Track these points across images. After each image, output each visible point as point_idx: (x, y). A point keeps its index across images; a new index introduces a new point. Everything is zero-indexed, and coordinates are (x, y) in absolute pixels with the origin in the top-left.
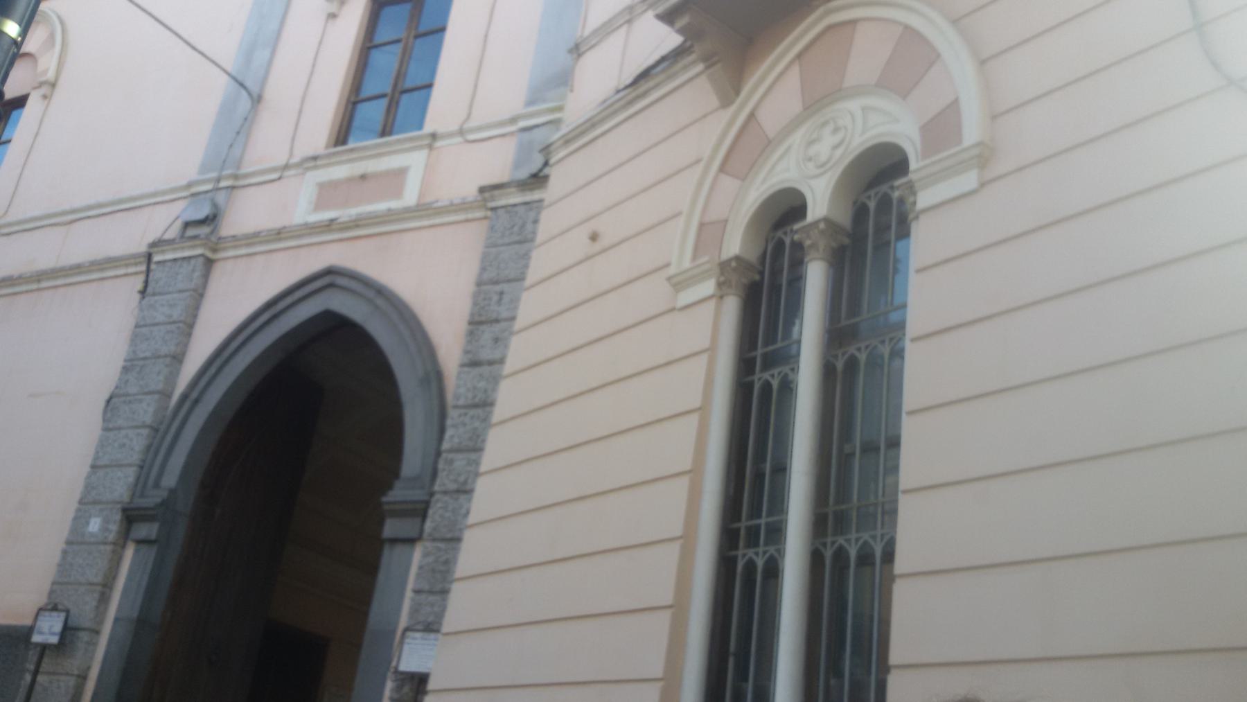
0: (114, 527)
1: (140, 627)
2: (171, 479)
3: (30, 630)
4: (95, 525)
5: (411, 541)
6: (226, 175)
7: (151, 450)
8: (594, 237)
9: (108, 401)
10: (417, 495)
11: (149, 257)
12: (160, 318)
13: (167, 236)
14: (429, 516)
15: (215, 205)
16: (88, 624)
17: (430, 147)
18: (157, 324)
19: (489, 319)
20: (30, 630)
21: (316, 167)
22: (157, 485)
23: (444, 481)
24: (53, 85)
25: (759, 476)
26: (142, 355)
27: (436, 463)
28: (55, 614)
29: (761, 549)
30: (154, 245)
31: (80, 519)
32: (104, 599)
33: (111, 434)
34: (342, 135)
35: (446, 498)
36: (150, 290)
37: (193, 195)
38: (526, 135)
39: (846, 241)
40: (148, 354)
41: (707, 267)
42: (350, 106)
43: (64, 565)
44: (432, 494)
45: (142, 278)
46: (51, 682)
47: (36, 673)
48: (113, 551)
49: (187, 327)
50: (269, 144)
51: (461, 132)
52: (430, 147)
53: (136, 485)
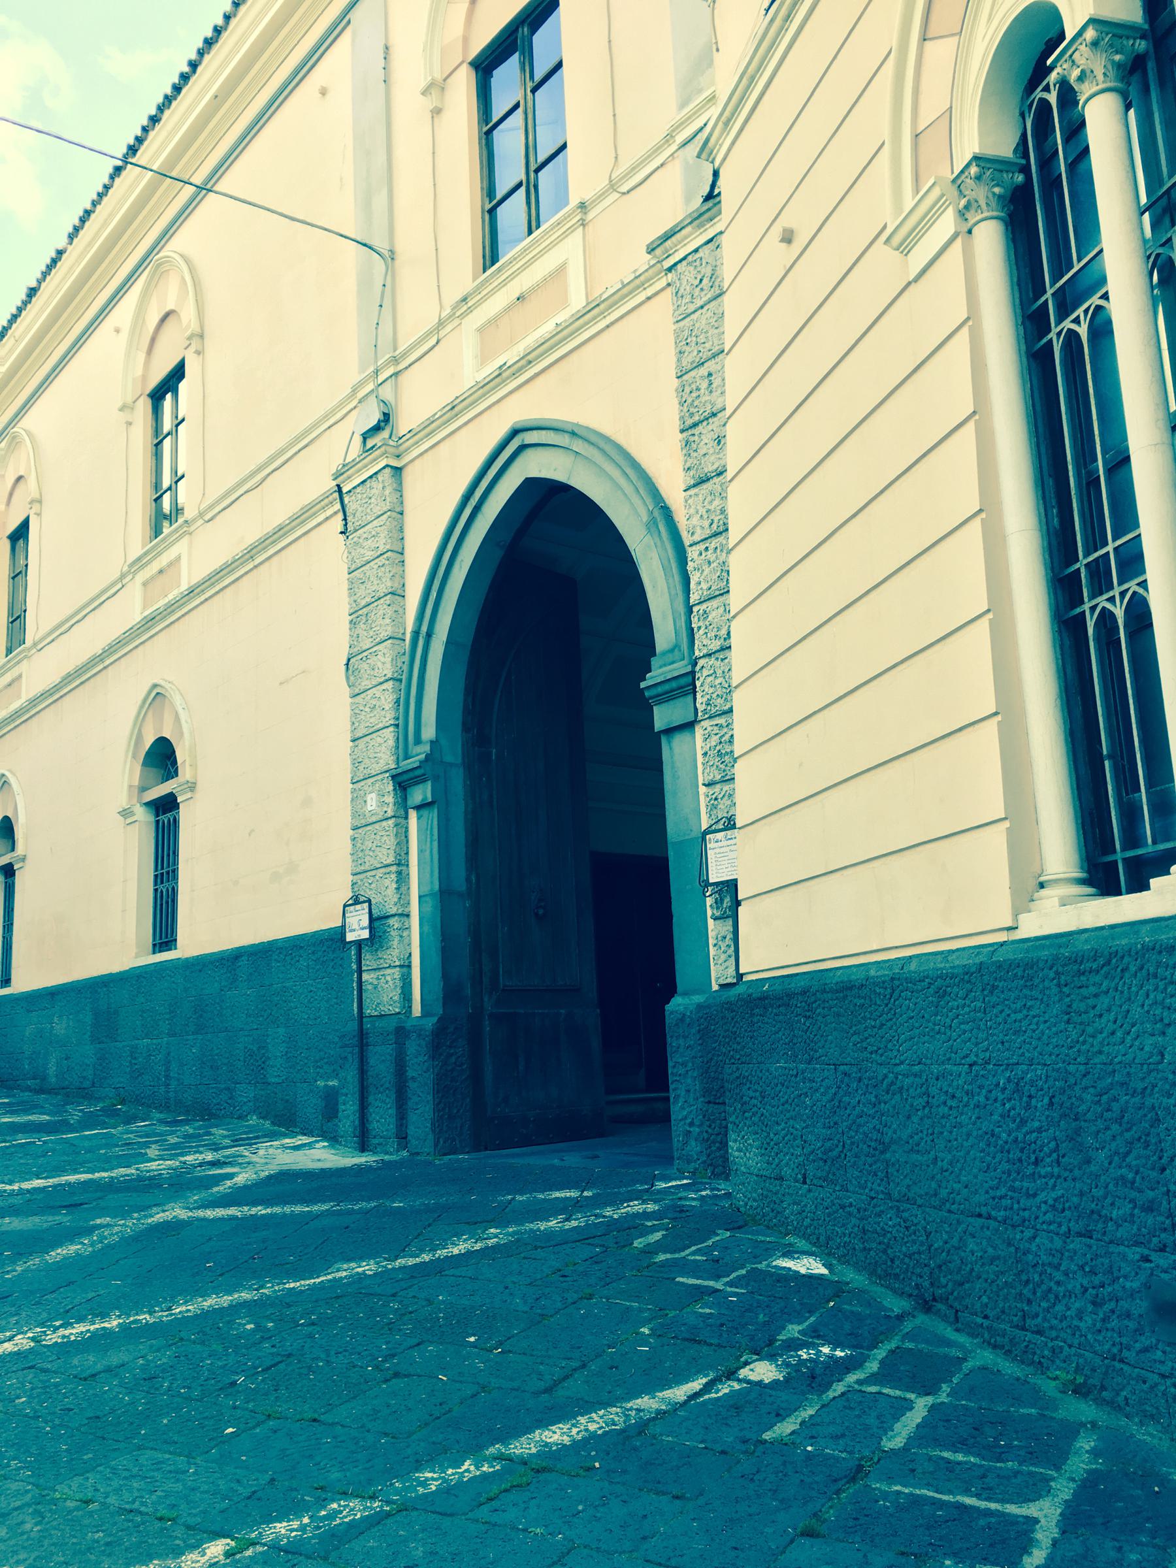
0: (390, 799)
1: (444, 896)
2: (429, 732)
5: (690, 726)
8: (788, 238)
9: (347, 664)
10: (680, 667)
12: (369, 555)
16: (394, 911)
17: (583, 224)
19: (699, 421)
21: (470, 310)
22: (418, 741)
23: (704, 642)
24: (201, 336)
25: (1092, 483)
26: (363, 603)
27: (689, 622)
28: (358, 907)
29: (1116, 592)
31: (357, 798)
32: (402, 879)
33: (359, 699)
34: (491, 255)
35: (712, 661)
36: (350, 527)
39: (1141, 46)
40: (368, 600)
41: (937, 192)
42: (487, 216)
45: (340, 516)
46: (378, 979)
47: (360, 971)
50: (417, 310)
51: (612, 186)
52: (583, 224)
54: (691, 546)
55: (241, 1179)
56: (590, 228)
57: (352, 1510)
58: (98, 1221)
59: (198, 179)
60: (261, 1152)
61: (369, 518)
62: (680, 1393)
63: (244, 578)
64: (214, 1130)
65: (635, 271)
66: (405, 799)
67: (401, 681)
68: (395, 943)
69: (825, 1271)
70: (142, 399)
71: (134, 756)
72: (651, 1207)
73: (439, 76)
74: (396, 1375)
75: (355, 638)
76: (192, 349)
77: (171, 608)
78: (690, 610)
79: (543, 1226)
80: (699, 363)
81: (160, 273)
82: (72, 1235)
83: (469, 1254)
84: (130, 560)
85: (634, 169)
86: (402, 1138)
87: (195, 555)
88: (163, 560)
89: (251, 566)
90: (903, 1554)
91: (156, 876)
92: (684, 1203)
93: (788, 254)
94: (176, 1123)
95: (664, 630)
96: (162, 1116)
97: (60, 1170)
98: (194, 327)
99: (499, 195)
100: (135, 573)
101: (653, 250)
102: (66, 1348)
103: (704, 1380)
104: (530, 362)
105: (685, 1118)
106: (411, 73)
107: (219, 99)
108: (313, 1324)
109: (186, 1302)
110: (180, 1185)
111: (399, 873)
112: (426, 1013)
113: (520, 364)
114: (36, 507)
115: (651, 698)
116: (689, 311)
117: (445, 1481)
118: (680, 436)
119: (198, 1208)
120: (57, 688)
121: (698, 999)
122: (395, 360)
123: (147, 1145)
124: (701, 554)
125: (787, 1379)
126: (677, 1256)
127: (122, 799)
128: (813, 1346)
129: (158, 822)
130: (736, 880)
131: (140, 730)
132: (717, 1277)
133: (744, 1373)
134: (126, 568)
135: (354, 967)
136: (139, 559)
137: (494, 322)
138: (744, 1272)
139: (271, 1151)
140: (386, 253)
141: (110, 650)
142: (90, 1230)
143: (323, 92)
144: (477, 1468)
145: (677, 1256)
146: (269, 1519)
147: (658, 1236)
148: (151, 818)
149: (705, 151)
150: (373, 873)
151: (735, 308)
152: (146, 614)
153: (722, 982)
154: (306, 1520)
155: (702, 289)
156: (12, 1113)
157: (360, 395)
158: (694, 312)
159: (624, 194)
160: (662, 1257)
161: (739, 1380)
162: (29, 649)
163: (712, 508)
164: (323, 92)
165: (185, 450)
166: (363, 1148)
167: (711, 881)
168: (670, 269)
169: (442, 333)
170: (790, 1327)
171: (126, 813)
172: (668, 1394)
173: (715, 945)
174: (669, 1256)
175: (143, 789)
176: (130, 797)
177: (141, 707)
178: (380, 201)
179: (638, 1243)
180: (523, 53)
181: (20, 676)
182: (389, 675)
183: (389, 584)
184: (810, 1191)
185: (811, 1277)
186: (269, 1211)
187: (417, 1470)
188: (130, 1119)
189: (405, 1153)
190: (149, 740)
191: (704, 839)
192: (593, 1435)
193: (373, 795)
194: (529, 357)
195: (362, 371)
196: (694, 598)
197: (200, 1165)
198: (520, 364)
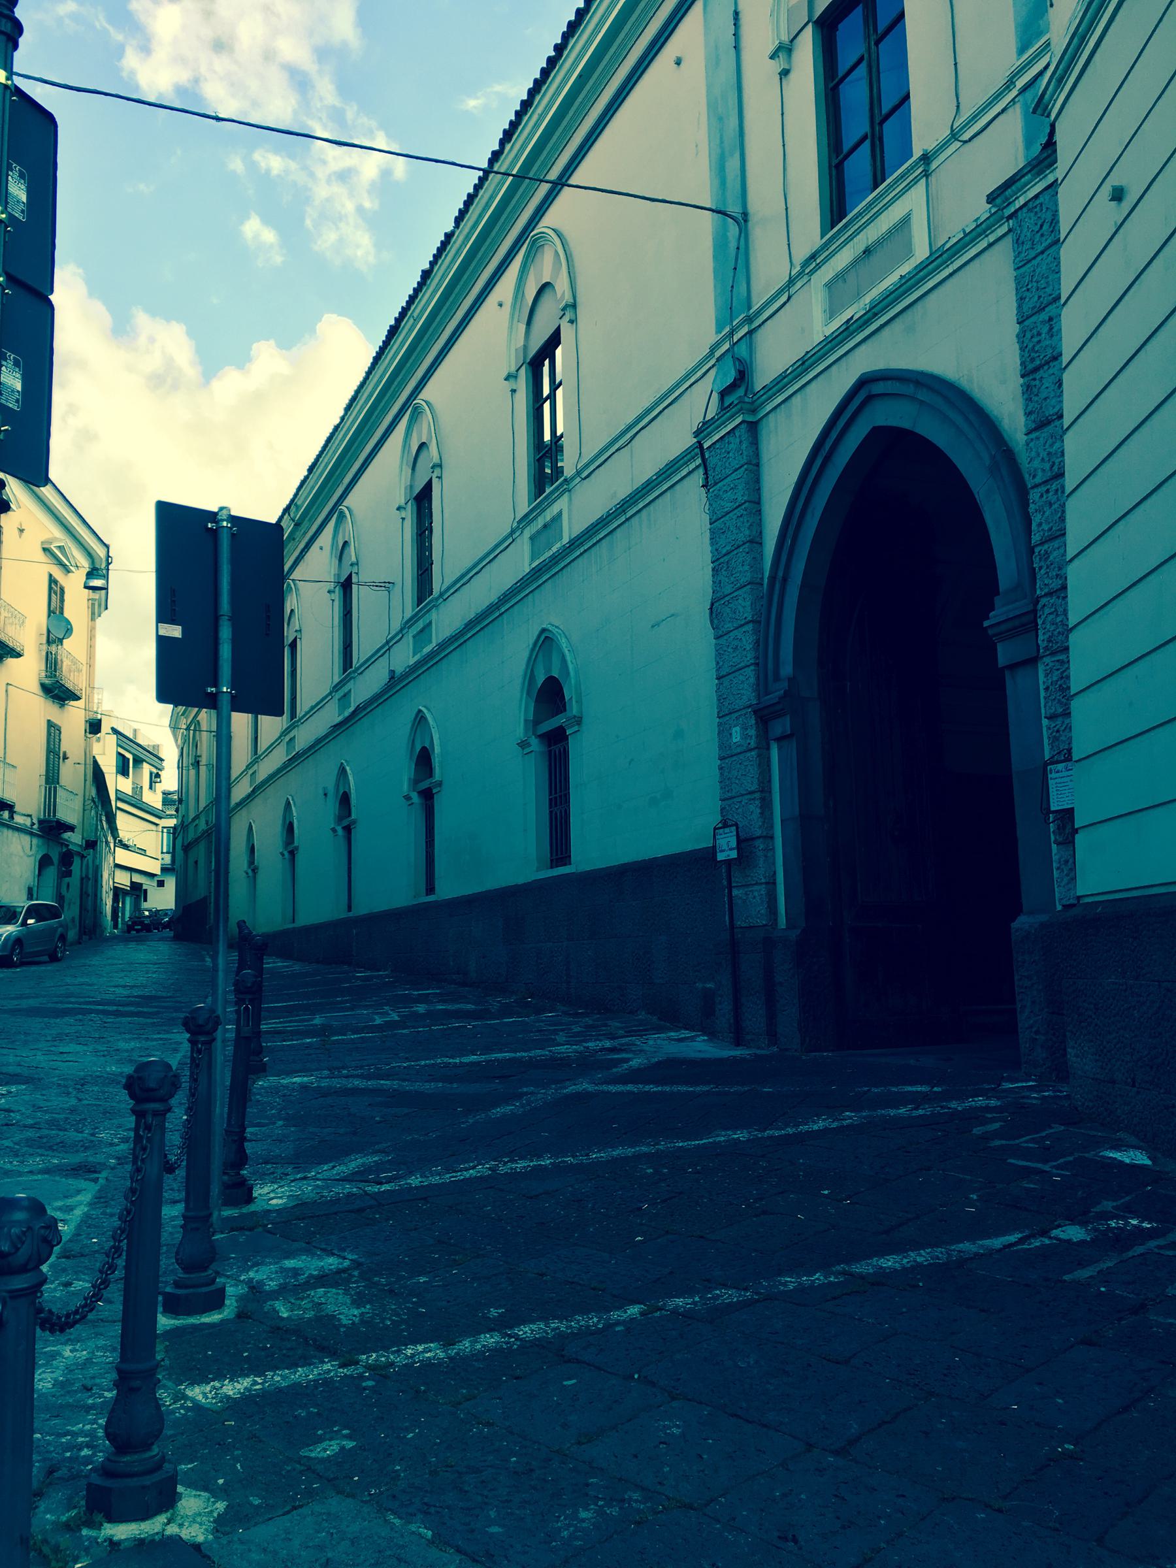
0: (752, 732)
1: (804, 823)
2: (787, 670)
4: (736, 735)
5: (1033, 661)
8: (1118, 195)
9: (711, 608)
10: (1022, 606)
12: (729, 506)
13: (708, 417)
14: (1038, 625)
15: (738, 360)
16: (758, 833)
17: (926, 174)
18: (727, 513)
19: (1040, 363)
21: (818, 267)
24: (574, 306)
26: (724, 551)
28: (727, 830)
30: (697, 434)
31: (723, 732)
32: (766, 804)
33: (722, 641)
34: (837, 207)
37: (718, 360)
38: (1029, 95)
40: (728, 548)
43: (725, 781)
44: (1037, 601)
45: (701, 471)
46: (746, 894)
48: (759, 756)
49: (755, 503)
50: (770, 266)
51: (954, 136)
53: (758, 685)
54: (1033, 488)
55: (635, 1062)
56: (933, 179)
57: (729, 1296)
58: (525, 1090)
60: (651, 1042)
61: (728, 472)
62: (997, 1243)
63: (618, 530)
64: (610, 1023)
65: (976, 220)
66: (766, 732)
67: (759, 622)
68: (761, 862)
69: (1149, 1162)
70: (523, 369)
71: (528, 693)
72: (993, 1103)
73: (785, 38)
74: (765, 1213)
75: (717, 583)
76: (567, 318)
77: (555, 559)
78: (1031, 551)
79: (892, 1112)
80: (1038, 309)
81: (536, 248)
82: (507, 1099)
83: (825, 1131)
84: (519, 515)
85: (975, 118)
86: (772, 1035)
87: (577, 510)
88: (548, 515)
89: (623, 519)
90: (1163, 1362)
91: (550, 800)
92: (1025, 1101)
93: (1116, 212)
94: (576, 1015)
95: (1006, 570)
96: (565, 1009)
98: (568, 298)
99: (846, 148)
100: (523, 529)
101: (994, 199)
102: (514, 1176)
103: (1020, 1236)
104: (876, 314)
105: (1031, 1027)
107: (583, 78)
108: (698, 1173)
109: (599, 1151)
110: (586, 1065)
111: (763, 799)
112: (791, 925)
113: (866, 317)
114: (437, 472)
115: (995, 635)
116: (1030, 257)
117: (800, 1284)
118: (1022, 381)
119: (602, 1084)
120: (461, 633)
121: (1044, 918)
122: (749, 320)
123: (555, 1032)
124: (1042, 496)
125: (1093, 1240)
126: (1012, 1142)
127: (520, 732)
128: (1124, 1218)
129: (550, 752)
130: (1072, 809)
131: (532, 671)
132: (1046, 1162)
133: (1054, 1233)
134: (515, 524)
135: (725, 883)
136: (526, 515)
137: (841, 276)
138: (1071, 1159)
139: (659, 1042)
140: (739, 217)
141: (505, 598)
142: (520, 1096)
143: (678, 62)
144: (826, 1278)
145: (1012, 1142)
147: (996, 1126)
149: (1041, 107)
150: (739, 799)
151: (1072, 258)
152: (533, 565)
153: (1065, 902)
154: (697, 1299)
155: (1042, 235)
156: (445, 1002)
157: (718, 354)
158: (1034, 258)
159: (965, 142)
160: (998, 1143)
161: (1050, 1238)
163: (1052, 450)
164: (678, 62)
165: (561, 418)
166: (738, 1042)
167: (1053, 808)
168: (1010, 217)
169: (792, 290)
170: (1105, 1203)
171: (523, 744)
172: (987, 1242)
173: (1058, 869)
174: (1004, 1142)
175: (536, 722)
176: (526, 729)
177: (533, 650)
178: (733, 164)
179: (977, 1131)
180: (866, 7)
181: (430, 623)
182: (749, 618)
183: (747, 532)
184: (1138, 1093)
185: (1134, 1167)
186: (660, 1088)
187: (779, 1275)
188: (539, 1011)
189: (775, 1049)
190: (540, 679)
191: (1045, 770)
192: (919, 1265)
193: (738, 729)
194: (875, 310)
195: (718, 332)
196: (1035, 538)
197: (601, 1050)
198: (866, 317)
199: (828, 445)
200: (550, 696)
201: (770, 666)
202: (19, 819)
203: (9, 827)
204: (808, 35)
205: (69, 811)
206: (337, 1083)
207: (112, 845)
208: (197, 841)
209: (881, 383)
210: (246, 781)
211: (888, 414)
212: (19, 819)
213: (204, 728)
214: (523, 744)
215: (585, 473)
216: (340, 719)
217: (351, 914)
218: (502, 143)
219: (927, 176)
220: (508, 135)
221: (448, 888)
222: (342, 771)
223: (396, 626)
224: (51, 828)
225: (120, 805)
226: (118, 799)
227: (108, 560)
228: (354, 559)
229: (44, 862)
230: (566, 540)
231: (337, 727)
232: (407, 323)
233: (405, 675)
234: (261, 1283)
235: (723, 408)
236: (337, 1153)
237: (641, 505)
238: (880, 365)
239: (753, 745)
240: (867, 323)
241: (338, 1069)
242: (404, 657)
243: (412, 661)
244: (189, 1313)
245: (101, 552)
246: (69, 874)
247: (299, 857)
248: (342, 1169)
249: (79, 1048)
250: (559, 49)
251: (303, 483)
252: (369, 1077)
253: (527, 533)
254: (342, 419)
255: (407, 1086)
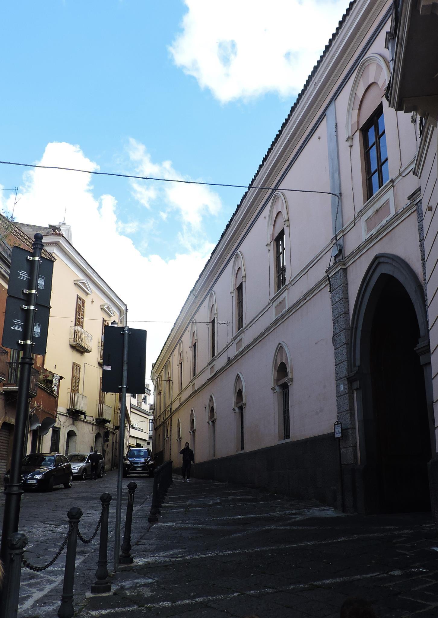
0: (347, 387)
1: (365, 422)
2: (358, 363)
3: (334, 433)
4: (342, 389)
6: (341, 233)
7: (349, 353)
11: (328, 276)
16: (349, 427)
17: (393, 186)
20: (334, 433)
22: (355, 366)
24: (288, 220)
30: (326, 272)
31: (338, 387)
32: (352, 415)
34: (369, 192)
45: (329, 285)
49: (346, 299)
50: (349, 213)
51: (400, 174)
52: (393, 186)
56: (395, 187)
59: (272, 187)
61: (337, 286)
70: (272, 242)
71: (275, 368)
73: (350, 135)
76: (286, 225)
77: (283, 316)
85: (406, 169)
87: (291, 296)
88: (281, 299)
97: (247, 514)
98: (286, 218)
100: (273, 303)
106: (344, 132)
107: (289, 141)
111: (351, 413)
114: (244, 279)
120: (252, 344)
122: (343, 231)
127: (272, 384)
137: (370, 218)
140: (338, 195)
141: (267, 330)
143: (319, 138)
146: (250, 590)
148: (281, 391)
162: (244, 329)
164: (319, 138)
166: (344, 511)
168: (416, 204)
169: (356, 222)
171: (273, 389)
177: (276, 351)
178: (337, 175)
199: (368, 279)
200: (282, 370)
201: (352, 361)
202: (88, 418)
203: (84, 421)
204: (358, 133)
205: (108, 415)
206: (182, 526)
207: (128, 428)
208: (160, 426)
209: (382, 258)
210: (178, 401)
211: (385, 269)
212: (88, 418)
213: (163, 379)
214: (273, 389)
215: (292, 283)
216: (211, 376)
217: (214, 458)
218: (263, 162)
219: (393, 187)
220: (265, 160)
221: (249, 448)
222: (211, 398)
223: (230, 340)
224: (101, 422)
225: (132, 410)
226: (131, 407)
227: (127, 311)
228: (216, 312)
229: (98, 436)
230: (287, 308)
231: (209, 380)
232: (233, 223)
233: (234, 359)
234: (125, 586)
235: (335, 262)
236: (167, 548)
237: (311, 297)
238: (382, 251)
239: (347, 392)
240: (377, 236)
241: (186, 521)
242: (233, 352)
243: (236, 354)
244: (98, 593)
245: (123, 308)
246: (107, 441)
247: (196, 434)
248: (167, 554)
249: (94, 512)
250: (280, 131)
251: (197, 281)
252: (194, 524)
253: (275, 304)
254: (211, 257)
255: (208, 527)
